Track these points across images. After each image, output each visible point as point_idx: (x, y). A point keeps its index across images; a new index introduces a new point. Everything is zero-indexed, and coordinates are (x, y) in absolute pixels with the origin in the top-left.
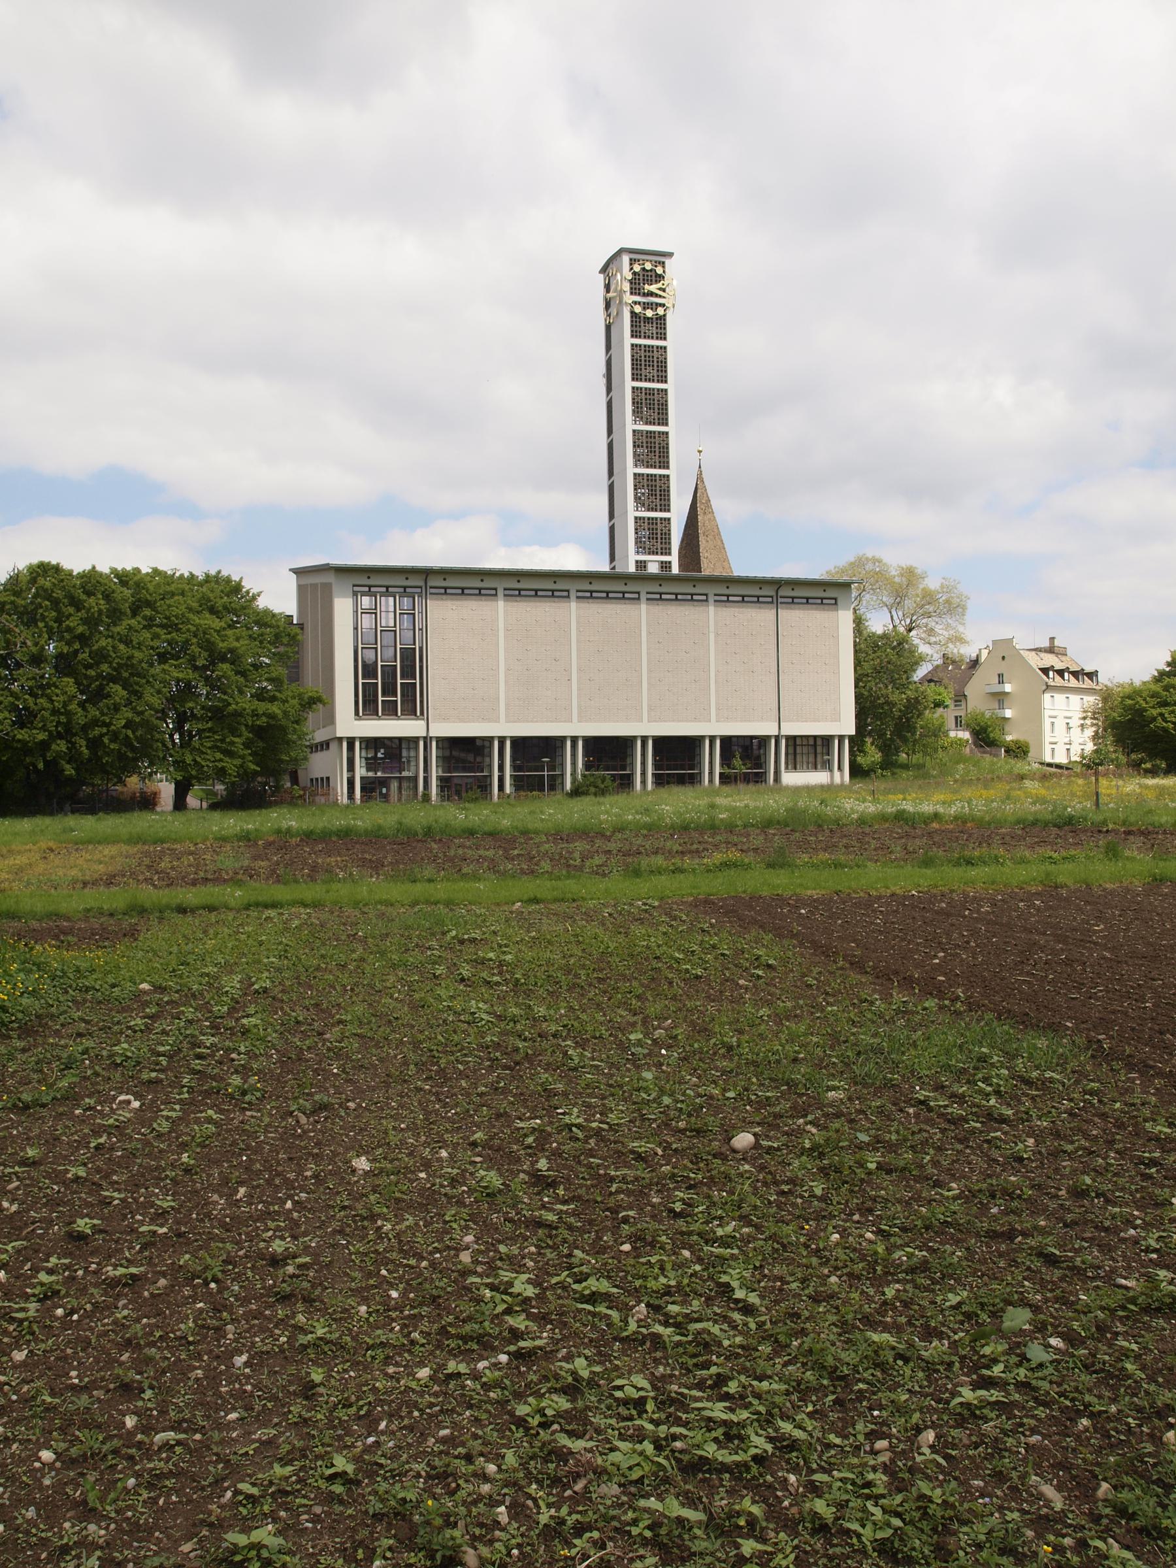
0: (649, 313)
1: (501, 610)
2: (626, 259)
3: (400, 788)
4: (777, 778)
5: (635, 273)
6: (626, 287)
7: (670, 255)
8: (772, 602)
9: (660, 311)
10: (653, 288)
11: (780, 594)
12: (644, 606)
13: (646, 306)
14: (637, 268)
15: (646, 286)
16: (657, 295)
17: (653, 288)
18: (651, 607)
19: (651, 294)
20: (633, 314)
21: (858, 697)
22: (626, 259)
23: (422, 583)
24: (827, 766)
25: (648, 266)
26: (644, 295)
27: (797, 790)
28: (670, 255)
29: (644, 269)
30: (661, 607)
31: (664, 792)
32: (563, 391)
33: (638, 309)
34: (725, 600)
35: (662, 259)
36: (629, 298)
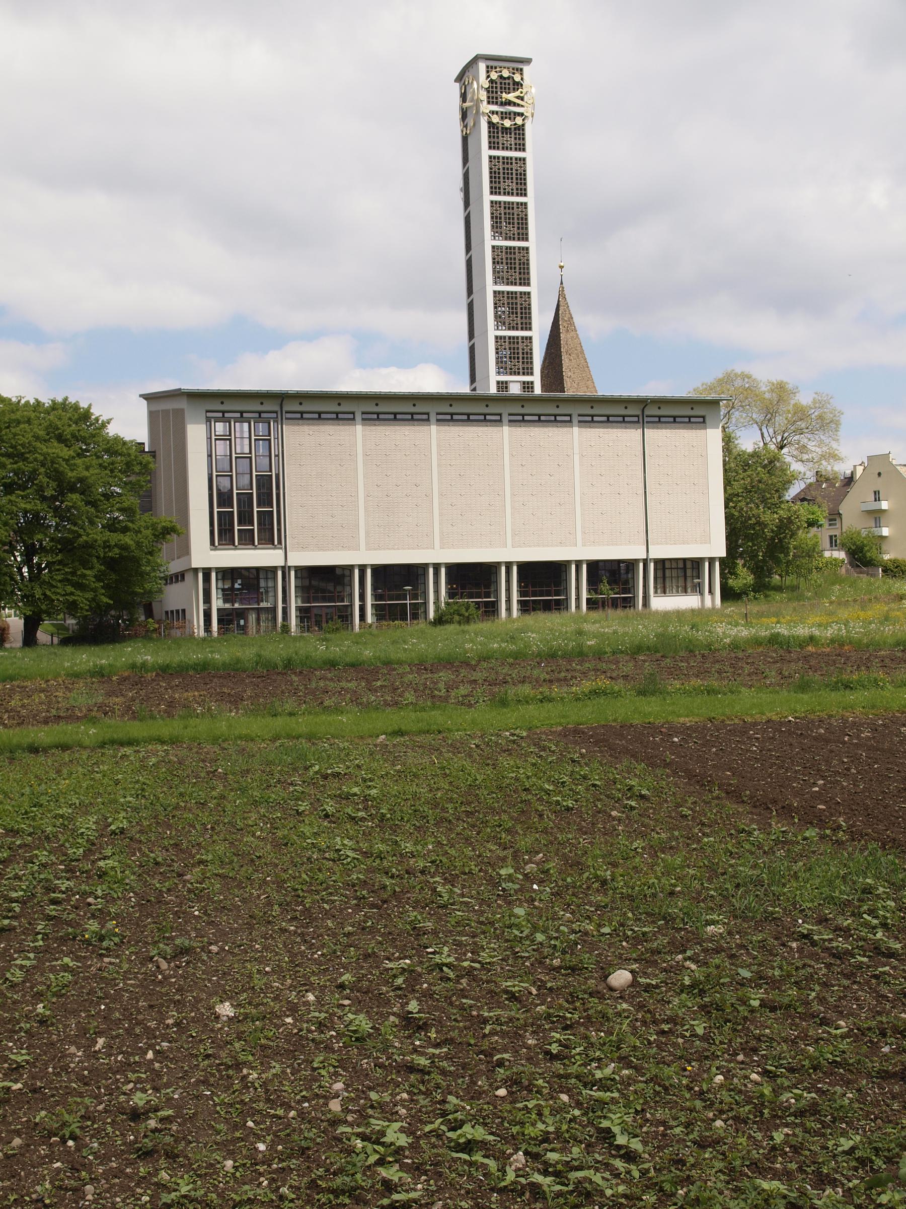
0: (507, 123)
1: (359, 435)
2: (482, 66)
3: (258, 620)
4: (646, 603)
5: (492, 81)
6: (483, 95)
7: (528, 61)
8: (638, 422)
9: (519, 121)
10: (511, 97)
11: (647, 412)
12: (576, 429)
13: (504, 116)
14: (494, 76)
15: (504, 95)
16: (515, 104)
17: (511, 97)
18: (513, 429)
19: (509, 103)
20: (491, 124)
21: (729, 518)
22: (482, 66)
23: (277, 408)
24: (698, 589)
25: (506, 73)
26: (503, 104)
27: (666, 615)
28: (528, 61)
29: (501, 77)
30: (523, 429)
31: (594, 615)
32: (416, 203)
33: (495, 119)
34: (589, 421)
35: (520, 66)
36: (486, 108)
